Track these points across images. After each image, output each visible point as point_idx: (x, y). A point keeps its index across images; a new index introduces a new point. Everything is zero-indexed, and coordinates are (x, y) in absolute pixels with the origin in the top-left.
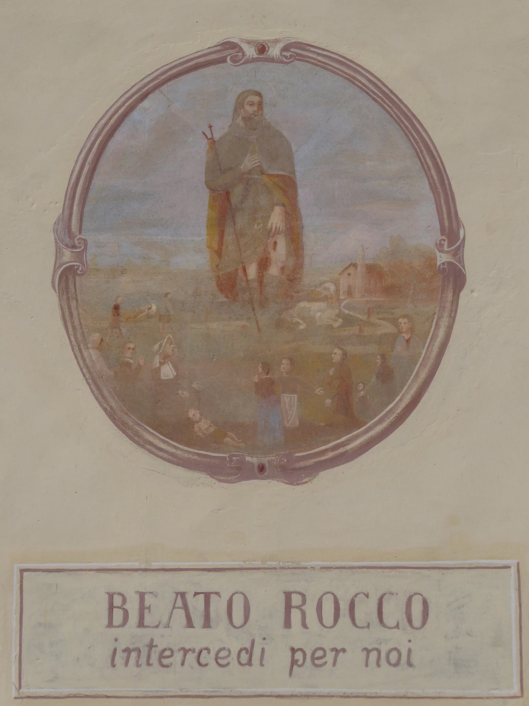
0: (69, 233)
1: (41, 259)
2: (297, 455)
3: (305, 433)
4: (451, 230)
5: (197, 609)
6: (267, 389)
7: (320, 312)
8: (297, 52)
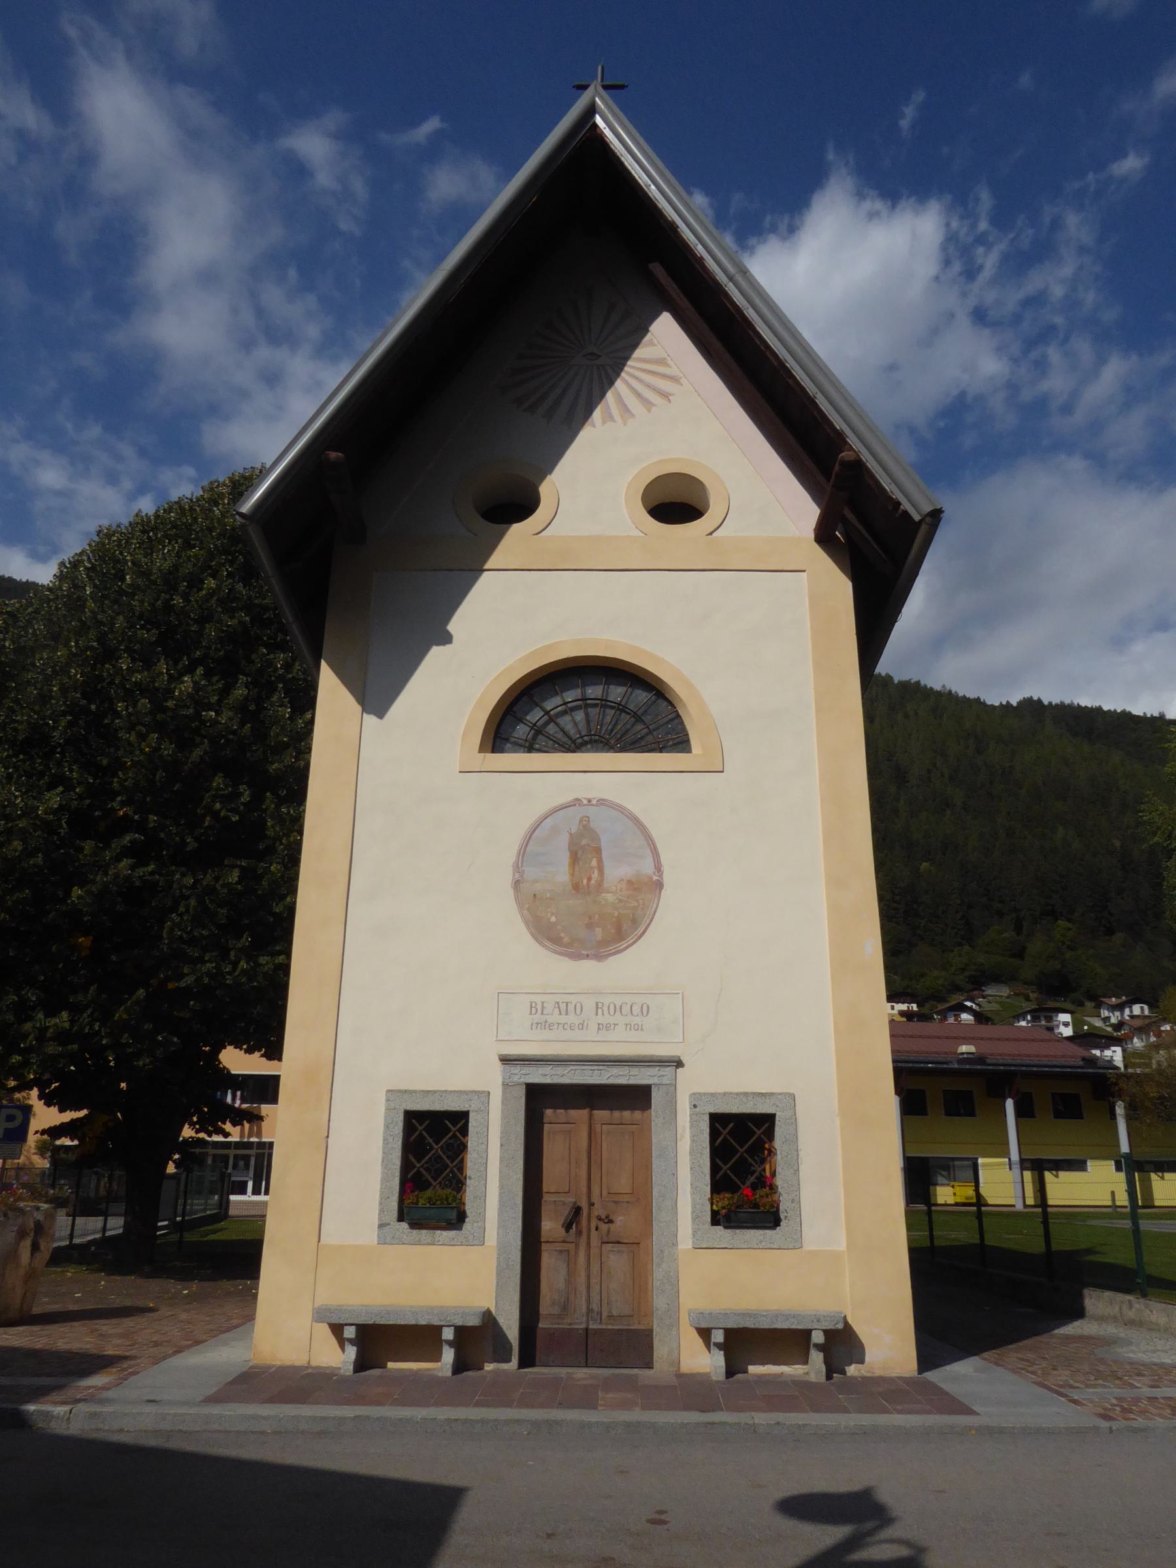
0: (518, 867)
3: (604, 943)
4: (658, 868)
5: (563, 1008)
6: (590, 926)
7: (610, 897)
8: (602, 802)
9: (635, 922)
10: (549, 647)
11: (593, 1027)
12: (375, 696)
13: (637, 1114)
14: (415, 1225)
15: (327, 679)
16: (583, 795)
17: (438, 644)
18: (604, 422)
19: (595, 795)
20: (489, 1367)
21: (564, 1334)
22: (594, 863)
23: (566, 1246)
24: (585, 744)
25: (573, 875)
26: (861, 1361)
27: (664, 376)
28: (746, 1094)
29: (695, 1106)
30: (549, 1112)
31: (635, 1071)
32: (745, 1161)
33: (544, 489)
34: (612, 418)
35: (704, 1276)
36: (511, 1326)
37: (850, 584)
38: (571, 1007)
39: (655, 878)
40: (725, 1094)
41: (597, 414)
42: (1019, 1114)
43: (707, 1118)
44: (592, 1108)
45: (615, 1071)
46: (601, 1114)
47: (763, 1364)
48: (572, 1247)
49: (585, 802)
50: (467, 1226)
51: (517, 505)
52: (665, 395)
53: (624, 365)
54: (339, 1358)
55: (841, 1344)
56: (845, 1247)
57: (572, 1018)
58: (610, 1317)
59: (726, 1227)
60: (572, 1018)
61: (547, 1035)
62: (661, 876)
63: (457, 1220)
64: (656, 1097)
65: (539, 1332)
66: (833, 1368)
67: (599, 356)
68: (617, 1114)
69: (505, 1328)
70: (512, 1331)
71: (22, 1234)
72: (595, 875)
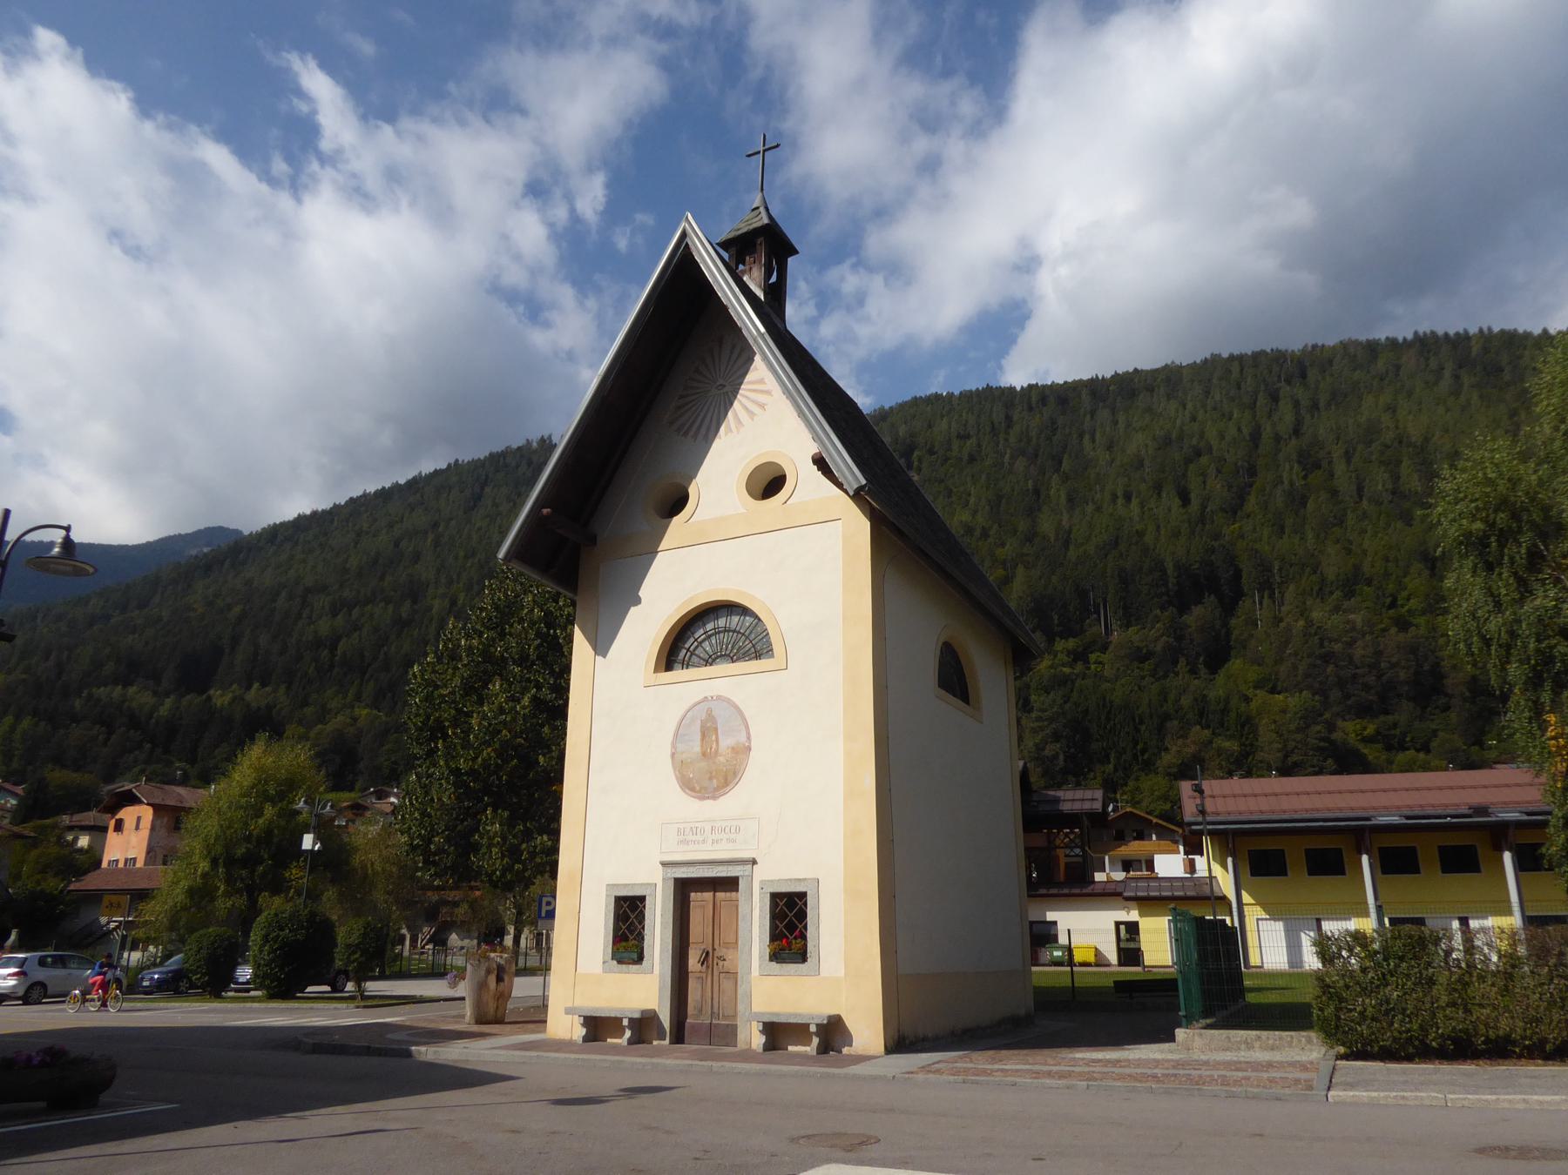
0: (674, 745)
1: (669, 751)
2: (501, 555)
3: (717, 789)
4: (749, 738)
5: (694, 831)
6: (711, 779)
7: (721, 759)
8: (719, 698)
9: (735, 774)
12: (601, 646)
14: (620, 962)
15: (579, 637)
16: (708, 694)
19: (714, 694)
21: (686, 1022)
27: (762, 392)
32: (790, 921)
33: (692, 490)
35: (767, 991)
41: (722, 429)
42: (1520, 867)
45: (692, 869)
46: (720, 895)
51: (676, 502)
52: (762, 406)
54: (579, 1032)
55: (832, 1034)
56: (845, 974)
63: (640, 959)
66: (825, 1048)
70: (666, 1024)
71: (489, 972)
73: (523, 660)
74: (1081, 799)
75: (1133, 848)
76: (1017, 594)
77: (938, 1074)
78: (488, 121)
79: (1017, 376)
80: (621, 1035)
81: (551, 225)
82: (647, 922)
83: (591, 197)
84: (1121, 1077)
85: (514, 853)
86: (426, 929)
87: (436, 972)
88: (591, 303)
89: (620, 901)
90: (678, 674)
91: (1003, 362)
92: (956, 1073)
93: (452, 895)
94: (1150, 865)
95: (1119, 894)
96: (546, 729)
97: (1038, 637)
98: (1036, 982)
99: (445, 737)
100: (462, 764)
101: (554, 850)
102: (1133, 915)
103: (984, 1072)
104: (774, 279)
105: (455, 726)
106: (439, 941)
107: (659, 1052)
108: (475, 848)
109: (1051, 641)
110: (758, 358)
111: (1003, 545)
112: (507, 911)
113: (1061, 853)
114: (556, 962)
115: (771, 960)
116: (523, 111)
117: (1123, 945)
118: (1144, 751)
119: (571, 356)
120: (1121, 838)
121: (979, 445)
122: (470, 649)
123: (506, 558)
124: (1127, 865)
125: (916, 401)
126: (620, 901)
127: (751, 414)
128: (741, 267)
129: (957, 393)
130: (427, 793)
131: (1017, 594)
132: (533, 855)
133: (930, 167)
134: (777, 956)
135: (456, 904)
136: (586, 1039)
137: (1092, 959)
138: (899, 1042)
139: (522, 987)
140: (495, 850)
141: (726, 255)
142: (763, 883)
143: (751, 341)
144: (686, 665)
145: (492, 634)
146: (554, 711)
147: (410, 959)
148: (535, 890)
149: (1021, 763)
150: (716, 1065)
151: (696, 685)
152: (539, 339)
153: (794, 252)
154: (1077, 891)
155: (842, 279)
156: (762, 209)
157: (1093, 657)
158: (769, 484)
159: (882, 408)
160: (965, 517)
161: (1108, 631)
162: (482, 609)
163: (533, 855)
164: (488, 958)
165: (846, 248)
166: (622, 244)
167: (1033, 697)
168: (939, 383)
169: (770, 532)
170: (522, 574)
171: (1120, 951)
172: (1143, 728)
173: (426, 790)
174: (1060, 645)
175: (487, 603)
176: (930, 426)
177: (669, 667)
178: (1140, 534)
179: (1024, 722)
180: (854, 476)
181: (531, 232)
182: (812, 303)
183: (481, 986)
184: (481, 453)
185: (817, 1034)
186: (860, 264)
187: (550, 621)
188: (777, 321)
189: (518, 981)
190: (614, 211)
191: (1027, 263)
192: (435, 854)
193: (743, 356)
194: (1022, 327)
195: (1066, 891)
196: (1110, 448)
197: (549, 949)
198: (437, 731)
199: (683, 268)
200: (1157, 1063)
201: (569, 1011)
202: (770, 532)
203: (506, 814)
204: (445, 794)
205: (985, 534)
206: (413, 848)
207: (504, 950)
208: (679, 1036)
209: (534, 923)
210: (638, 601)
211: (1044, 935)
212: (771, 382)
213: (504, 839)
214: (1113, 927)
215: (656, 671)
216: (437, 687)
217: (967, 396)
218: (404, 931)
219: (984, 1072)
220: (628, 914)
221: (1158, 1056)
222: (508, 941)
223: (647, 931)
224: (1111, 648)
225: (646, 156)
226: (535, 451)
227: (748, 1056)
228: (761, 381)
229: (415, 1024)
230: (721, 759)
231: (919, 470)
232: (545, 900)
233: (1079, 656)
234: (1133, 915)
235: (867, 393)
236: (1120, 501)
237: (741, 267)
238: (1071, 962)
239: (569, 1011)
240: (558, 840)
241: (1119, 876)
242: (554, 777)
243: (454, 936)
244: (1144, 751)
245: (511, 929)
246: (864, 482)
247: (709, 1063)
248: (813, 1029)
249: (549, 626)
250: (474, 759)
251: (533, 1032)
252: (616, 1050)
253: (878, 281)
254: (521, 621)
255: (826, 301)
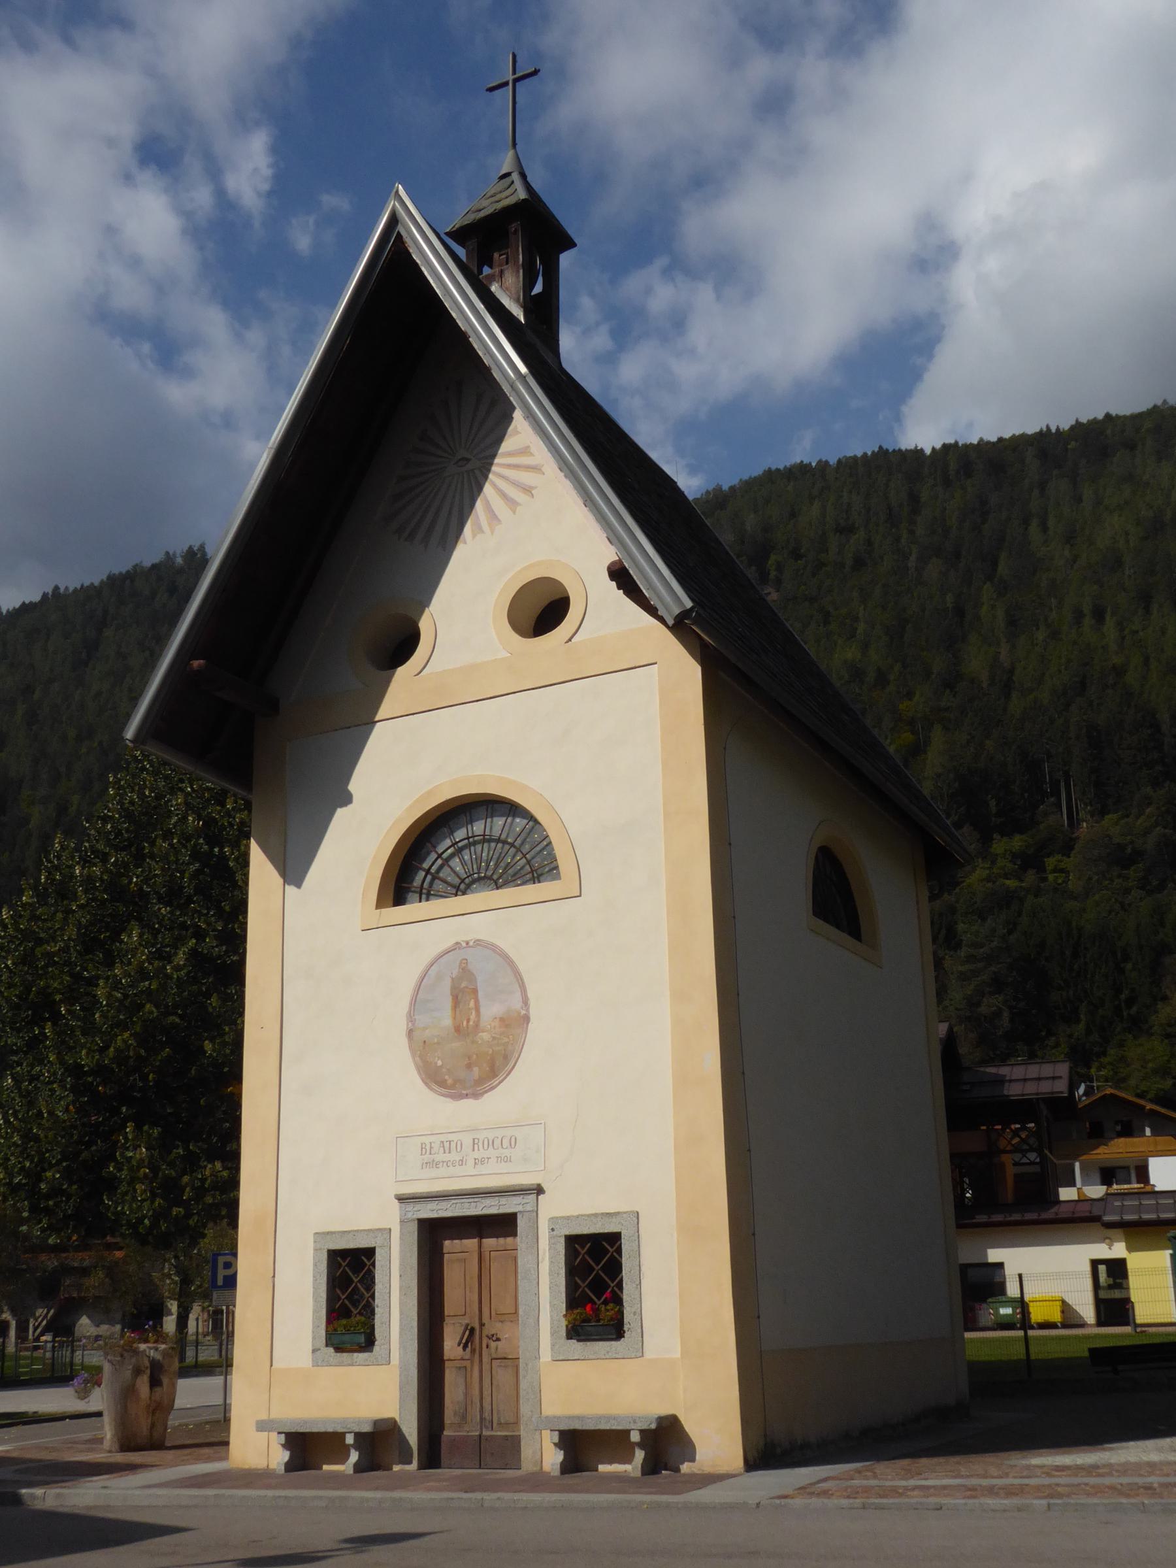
0: (411, 1017)
2: (130, 733)
3: (480, 1081)
4: (526, 1002)
5: (447, 1147)
6: (469, 1066)
7: (485, 1036)
8: (478, 943)
9: (506, 1058)
10: (430, 793)
11: (471, 1162)
12: (293, 869)
13: (510, 1240)
14: (338, 1349)
15: (256, 854)
16: (462, 938)
17: (341, 806)
18: (474, 536)
19: (471, 937)
20: (396, 1468)
21: (444, 1434)
22: (472, 1004)
23: (464, 1363)
24: (468, 886)
25: (455, 1018)
26: (693, 1460)
28: (596, 1215)
29: (553, 1230)
30: (447, 1243)
31: (503, 1201)
32: (597, 1277)
33: (424, 625)
34: (481, 530)
35: (567, 1384)
36: (411, 1431)
37: (699, 668)
38: (453, 1145)
39: (523, 1012)
40: (578, 1217)
43: (563, 1240)
44: (481, 1237)
45: (488, 1202)
46: (489, 1242)
47: (611, 1463)
48: (468, 1364)
49: (464, 945)
50: (376, 1348)
51: (401, 644)
52: (528, 490)
53: (491, 464)
54: (279, 1457)
55: (664, 1444)
56: (681, 1351)
57: (454, 1156)
58: (500, 1424)
59: (579, 1341)
60: (454, 1156)
61: (434, 1173)
62: (528, 1010)
63: (368, 1343)
64: (521, 1222)
65: (443, 1439)
66: (653, 1467)
67: (468, 460)
68: (501, 1240)
69: (407, 1435)
71: (137, 1372)
72: (473, 1017)
73: (173, 895)
74: (1037, 1077)
75: (1117, 1149)
76: (932, 770)
77: (821, 1497)
78: (68, 40)
79: (923, 433)
80: (343, 1459)
81: (186, 214)
82: (379, 1288)
83: (250, 166)
84: (1098, 1490)
85: (170, 1190)
86: (40, 1312)
87: (56, 1376)
88: (256, 336)
89: (336, 1257)
90: (412, 909)
91: (905, 409)
92: (853, 1494)
93: (77, 1259)
94: (1143, 1173)
95: (1093, 1219)
96: (214, 1001)
97: (967, 837)
98: (971, 1354)
99: (56, 1017)
100: (85, 1059)
101: (233, 1184)
102: (1118, 1250)
103: (895, 1492)
104: (538, 288)
105: (70, 1000)
106: (62, 1328)
107: (404, 1482)
108: (111, 1185)
109: (986, 840)
110: (518, 415)
111: (910, 695)
112: (166, 1277)
113: (1007, 1159)
114: (241, 1352)
115: (569, 1337)
116: (125, 24)
117: (1103, 1295)
118: (1130, 1002)
119: (228, 421)
120: (1098, 1134)
121: (869, 542)
122: (88, 881)
123: (139, 738)
124: (1108, 1175)
125: (771, 476)
126: (336, 1257)
127: (512, 504)
128: (487, 270)
129: (833, 461)
130: (31, 1104)
131: (932, 770)
132: (200, 1192)
133: (775, 104)
134: (579, 1330)
135: (85, 1272)
136: (290, 1467)
137: (1056, 1317)
138: (764, 1453)
139: (190, 1393)
140: (140, 1187)
141: (461, 252)
142: (553, 1220)
143: (506, 388)
144: (426, 894)
145: (123, 856)
146: (224, 972)
147: (17, 1358)
148: (207, 1244)
149: (943, 1028)
150: (489, 1497)
151: (438, 926)
152: (177, 394)
153: (569, 244)
154: (1029, 1216)
155: (649, 291)
156: (515, 177)
157: (1050, 862)
158: (542, 610)
159: (718, 490)
160: (851, 653)
161: (1073, 822)
162: (105, 819)
163: (200, 1192)
164: (136, 1352)
165: (651, 239)
166: (303, 242)
167: (961, 927)
168: (804, 449)
169: (546, 686)
170: (165, 763)
171: (1099, 1303)
172: (1129, 966)
173: (30, 1100)
174: (999, 846)
175: (112, 809)
176: (793, 515)
177: (399, 899)
178: (1120, 671)
179: (948, 963)
180: (674, 596)
181: (153, 221)
182: (604, 329)
183: (126, 1395)
184: (95, 578)
185: (641, 1445)
186: (680, 267)
187: (213, 833)
188: (549, 359)
189: (183, 1384)
190: (289, 190)
191: (932, 254)
192: (48, 1197)
193: (496, 413)
194: (930, 356)
195: (1017, 1217)
196: (1070, 538)
197: (231, 1335)
198: (44, 1009)
199: (395, 268)
200: (1152, 1466)
201: (262, 1426)
202: (546, 686)
203: (156, 1132)
204: (60, 1104)
205: (882, 679)
206: (14, 1189)
207: (161, 1337)
208: (432, 1456)
209: (207, 1296)
210: (347, 799)
211: (985, 1284)
212: (541, 454)
213: (155, 1169)
214: (1087, 1268)
215: (380, 904)
216: (39, 942)
217: (849, 466)
218: (7, 1316)
219: (895, 1492)
220: (349, 1277)
221: (1155, 1457)
222: (170, 1324)
223: (378, 1301)
224: (1077, 847)
225: (324, 99)
226: (181, 571)
227: (538, 1482)
228: (525, 451)
229: (28, 1456)
230: (485, 1036)
231: (778, 582)
232: (221, 1260)
233: (1030, 861)
234: (1118, 1250)
235: (693, 470)
236: (1088, 621)
237: (487, 270)
238: (1024, 1322)
239: (262, 1426)
240: (237, 1169)
241: (1096, 1191)
242: (229, 1072)
243: (84, 1320)
244: (1130, 1002)
245: (173, 1306)
246: (689, 604)
247: (478, 1495)
248: (635, 1437)
249: (213, 841)
250: (103, 1050)
251: (209, 1459)
252: (338, 1481)
253: (705, 294)
254: (168, 835)
255: (626, 326)
